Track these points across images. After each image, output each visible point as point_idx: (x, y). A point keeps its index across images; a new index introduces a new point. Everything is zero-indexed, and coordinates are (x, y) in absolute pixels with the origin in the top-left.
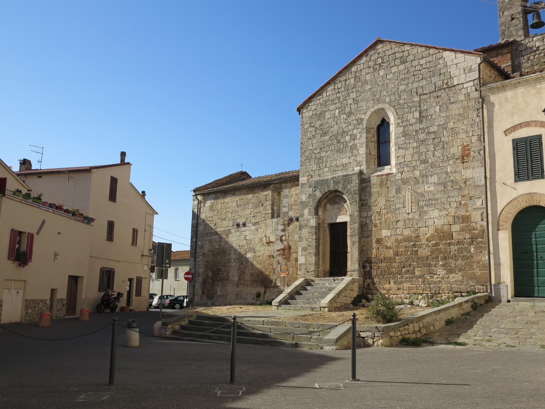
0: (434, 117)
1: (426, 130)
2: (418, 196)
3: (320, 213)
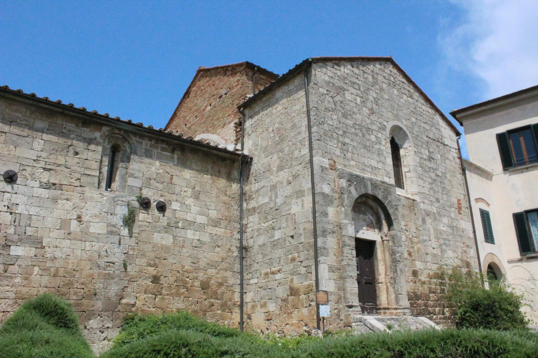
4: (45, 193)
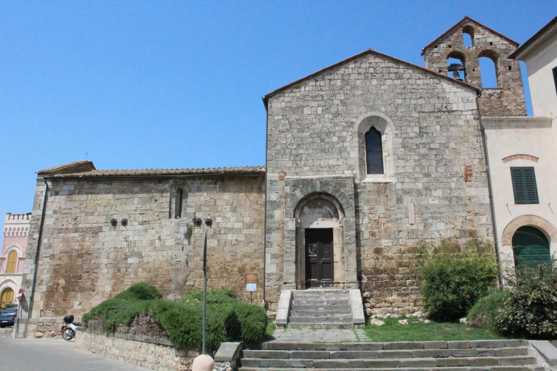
0: (434, 135)
1: (427, 146)
2: (420, 211)
3: (297, 216)
4: (141, 227)
